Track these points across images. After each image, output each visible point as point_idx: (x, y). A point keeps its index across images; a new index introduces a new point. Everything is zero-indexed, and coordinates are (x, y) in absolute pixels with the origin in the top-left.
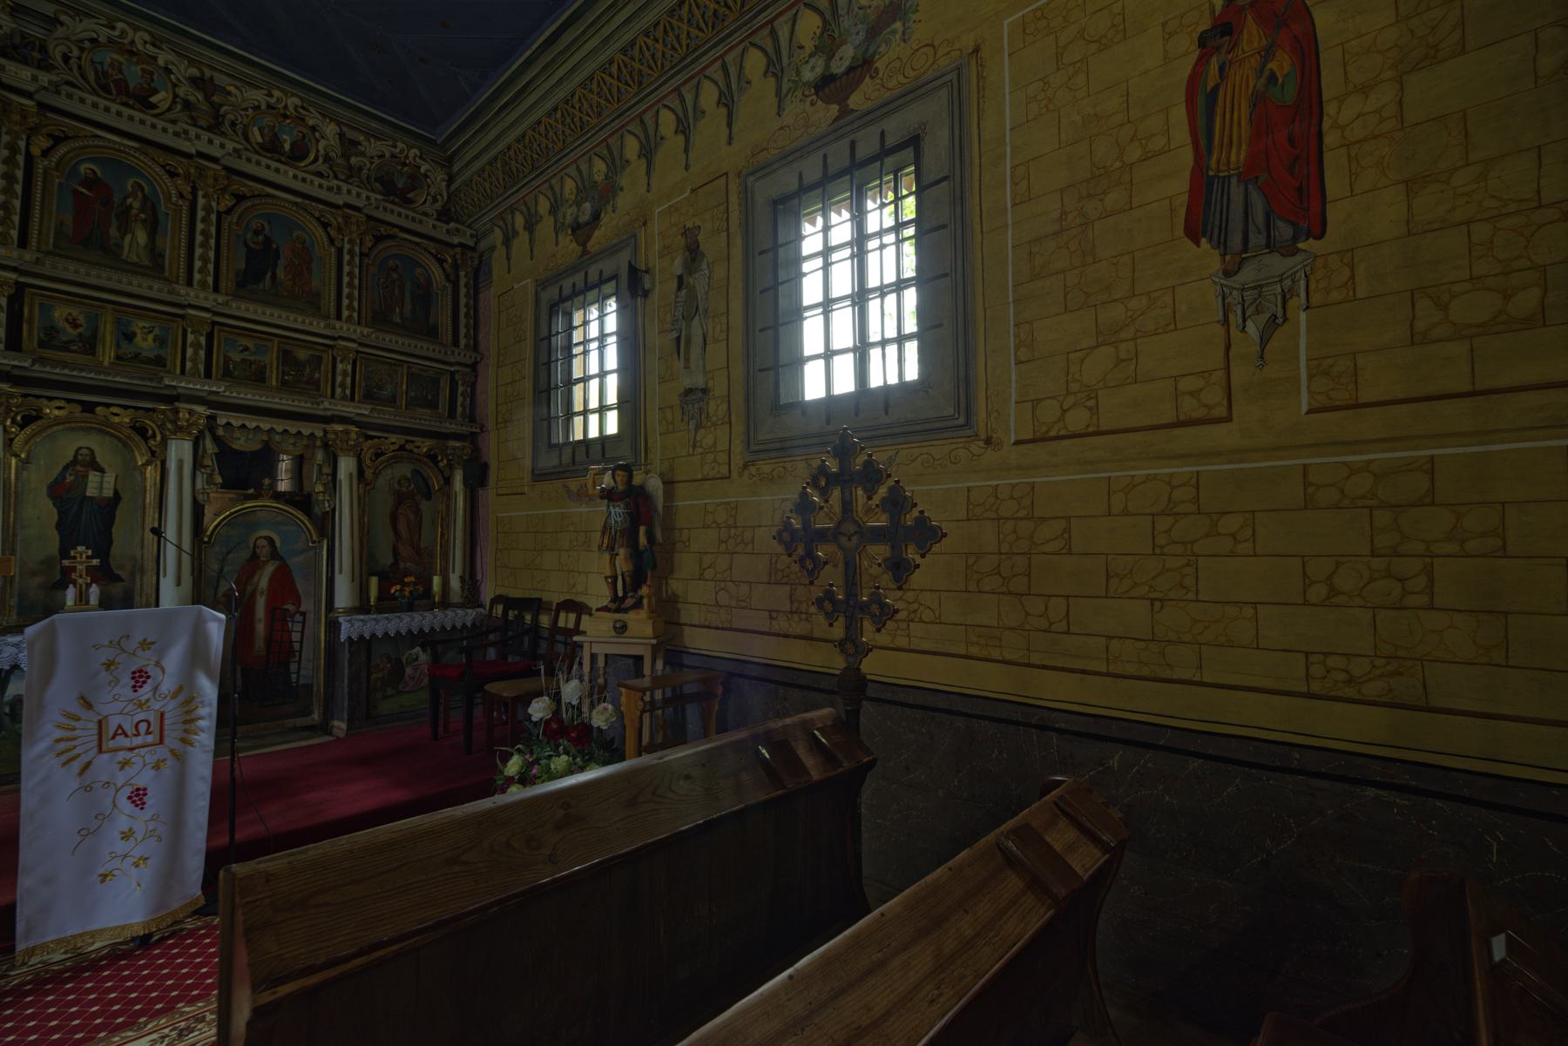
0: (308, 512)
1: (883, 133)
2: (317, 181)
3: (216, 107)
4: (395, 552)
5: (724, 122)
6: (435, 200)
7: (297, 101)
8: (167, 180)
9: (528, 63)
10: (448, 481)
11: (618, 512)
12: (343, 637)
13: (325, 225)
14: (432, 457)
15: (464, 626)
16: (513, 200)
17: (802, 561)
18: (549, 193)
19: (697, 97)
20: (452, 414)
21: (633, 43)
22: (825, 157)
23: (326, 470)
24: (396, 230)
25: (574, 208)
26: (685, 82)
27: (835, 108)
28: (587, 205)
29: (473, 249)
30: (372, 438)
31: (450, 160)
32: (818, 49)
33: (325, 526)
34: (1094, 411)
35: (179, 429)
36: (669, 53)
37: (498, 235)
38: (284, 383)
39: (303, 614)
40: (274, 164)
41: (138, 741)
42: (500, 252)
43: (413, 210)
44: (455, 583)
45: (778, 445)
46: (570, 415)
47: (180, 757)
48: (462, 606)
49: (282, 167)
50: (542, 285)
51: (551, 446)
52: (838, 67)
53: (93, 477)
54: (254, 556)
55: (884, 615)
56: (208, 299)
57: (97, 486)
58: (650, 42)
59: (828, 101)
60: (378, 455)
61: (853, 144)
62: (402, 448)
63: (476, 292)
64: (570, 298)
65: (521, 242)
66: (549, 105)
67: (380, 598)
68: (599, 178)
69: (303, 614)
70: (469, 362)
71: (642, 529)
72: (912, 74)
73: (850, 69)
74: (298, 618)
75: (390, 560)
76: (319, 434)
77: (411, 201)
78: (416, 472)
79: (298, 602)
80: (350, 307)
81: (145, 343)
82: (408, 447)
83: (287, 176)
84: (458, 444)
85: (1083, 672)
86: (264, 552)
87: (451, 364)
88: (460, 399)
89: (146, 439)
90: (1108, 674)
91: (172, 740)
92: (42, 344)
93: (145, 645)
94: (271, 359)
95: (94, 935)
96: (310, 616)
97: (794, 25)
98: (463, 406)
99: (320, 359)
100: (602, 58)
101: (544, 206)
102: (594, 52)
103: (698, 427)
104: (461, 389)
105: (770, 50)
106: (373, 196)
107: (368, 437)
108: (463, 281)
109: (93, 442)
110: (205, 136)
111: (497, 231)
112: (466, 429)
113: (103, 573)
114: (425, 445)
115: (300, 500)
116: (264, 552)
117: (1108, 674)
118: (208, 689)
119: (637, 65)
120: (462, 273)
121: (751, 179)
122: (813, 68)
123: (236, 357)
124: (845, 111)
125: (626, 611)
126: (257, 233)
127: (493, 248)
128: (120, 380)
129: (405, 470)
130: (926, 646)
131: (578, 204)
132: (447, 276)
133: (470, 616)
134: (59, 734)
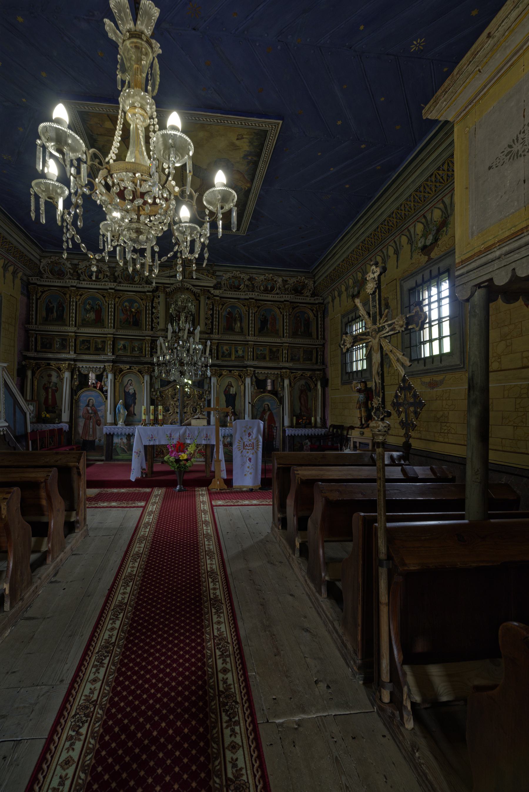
0: (277, 396)
1: (439, 268)
2: (277, 296)
3: (253, 284)
4: (301, 409)
5: (396, 260)
6: (310, 291)
7: (271, 275)
8: (243, 307)
9: (335, 247)
10: (316, 385)
11: (361, 397)
12: (287, 435)
13: (279, 308)
14: (311, 377)
15: (321, 434)
16: (334, 287)
17: (396, 412)
18: (345, 284)
19: (387, 251)
20: (317, 363)
21: (365, 240)
22: (423, 275)
23: (281, 384)
24: (298, 304)
25: (352, 289)
26: (383, 248)
27: (427, 257)
28: (356, 288)
29: (322, 303)
30: (293, 373)
31: (314, 276)
32: (423, 235)
33: (281, 401)
34: (500, 363)
35: (248, 375)
36: (376, 241)
37: (330, 299)
38: (270, 359)
39: (276, 427)
40: (266, 295)
41: (250, 448)
42: (330, 305)
43: (304, 296)
44: (319, 420)
45: (411, 374)
46: (352, 362)
47: (256, 453)
48: (321, 428)
49: (268, 295)
50: (343, 316)
51: (347, 373)
52: (428, 243)
53: (232, 389)
54: (264, 410)
55: (414, 427)
56: (73, 329)
57: (233, 391)
58: (370, 239)
59: (425, 255)
60: (295, 378)
61: (431, 271)
62: (302, 375)
63: (324, 318)
64: (351, 322)
65: (337, 300)
66: (342, 259)
67: (296, 424)
68: (360, 278)
69: (276, 427)
70: (322, 343)
71: (369, 402)
72: (448, 246)
73: (431, 244)
74: (275, 428)
75: (299, 412)
76: (279, 373)
77: (303, 293)
78: (306, 383)
79: (275, 424)
80: (286, 333)
81: (240, 353)
82: (304, 375)
83: (269, 297)
84: (318, 372)
85: (496, 450)
86: (267, 408)
87: (316, 345)
88: (319, 357)
89: (241, 378)
90: (502, 451)
91: (255, 448)
92: (222, 357)
93: (250, 427)
94: (267, 352)
95: (245, 487)
96: (278, 428)
97: (415, 227)
98: (320, 359)
99: (279, 350)
100: (356, 245)
101: (343, 288)
102: (354, 242)
103: (389, 367)
104: (319, 353)
105: (408, 236)
106: (292, 296)
107: (292, 373)
108: (319, 316)
109: (231, 380)
110: (251, 293)
111: (330, 297)
112: (321, 367)
113: (234, 414)
114: (309, 374)
115: (274, 392)
116: (267, 408)
117: (502, 451)
118: (261, 439)
119: (367, 246)
120: (319, 313)
121: (402, 282)
122: (421, 242)
123: (259, 353)
124: (430, 259)
125: (364, 428)
126: (263, 316)
127: (329, 303)
128: (236, 363)
129: (303, 382)
130: (454, 441)
131: (354, 288)
132: (314, 315)
133: (323, 431)
134: (238, 444)
